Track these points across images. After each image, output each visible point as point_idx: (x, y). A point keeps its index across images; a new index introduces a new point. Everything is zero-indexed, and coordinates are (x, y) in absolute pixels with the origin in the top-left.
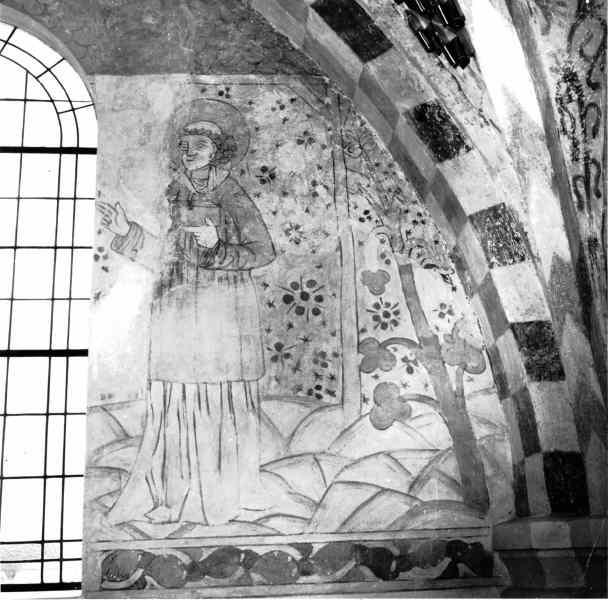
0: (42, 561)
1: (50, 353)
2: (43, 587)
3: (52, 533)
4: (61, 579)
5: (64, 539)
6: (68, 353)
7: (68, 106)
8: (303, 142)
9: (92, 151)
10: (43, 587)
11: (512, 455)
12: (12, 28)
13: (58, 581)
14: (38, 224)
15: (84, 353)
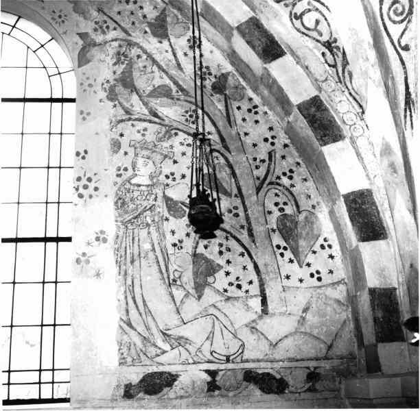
0: (40, 383)
1: (46, 240)
2: (40, 401)
3: (47, 364)
4: (40, 397)
5: (38, 372)
6: (57, 240)
7: (55, 71)
8: (261, 161)
9: (73, 100)
10: (40, 401)
11: (383, 43)
12: (17, 18)
13: (51, 397)
14: (36, 152)
15: (69, 239)
